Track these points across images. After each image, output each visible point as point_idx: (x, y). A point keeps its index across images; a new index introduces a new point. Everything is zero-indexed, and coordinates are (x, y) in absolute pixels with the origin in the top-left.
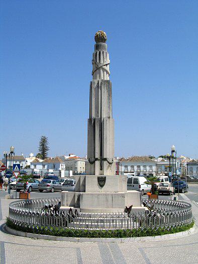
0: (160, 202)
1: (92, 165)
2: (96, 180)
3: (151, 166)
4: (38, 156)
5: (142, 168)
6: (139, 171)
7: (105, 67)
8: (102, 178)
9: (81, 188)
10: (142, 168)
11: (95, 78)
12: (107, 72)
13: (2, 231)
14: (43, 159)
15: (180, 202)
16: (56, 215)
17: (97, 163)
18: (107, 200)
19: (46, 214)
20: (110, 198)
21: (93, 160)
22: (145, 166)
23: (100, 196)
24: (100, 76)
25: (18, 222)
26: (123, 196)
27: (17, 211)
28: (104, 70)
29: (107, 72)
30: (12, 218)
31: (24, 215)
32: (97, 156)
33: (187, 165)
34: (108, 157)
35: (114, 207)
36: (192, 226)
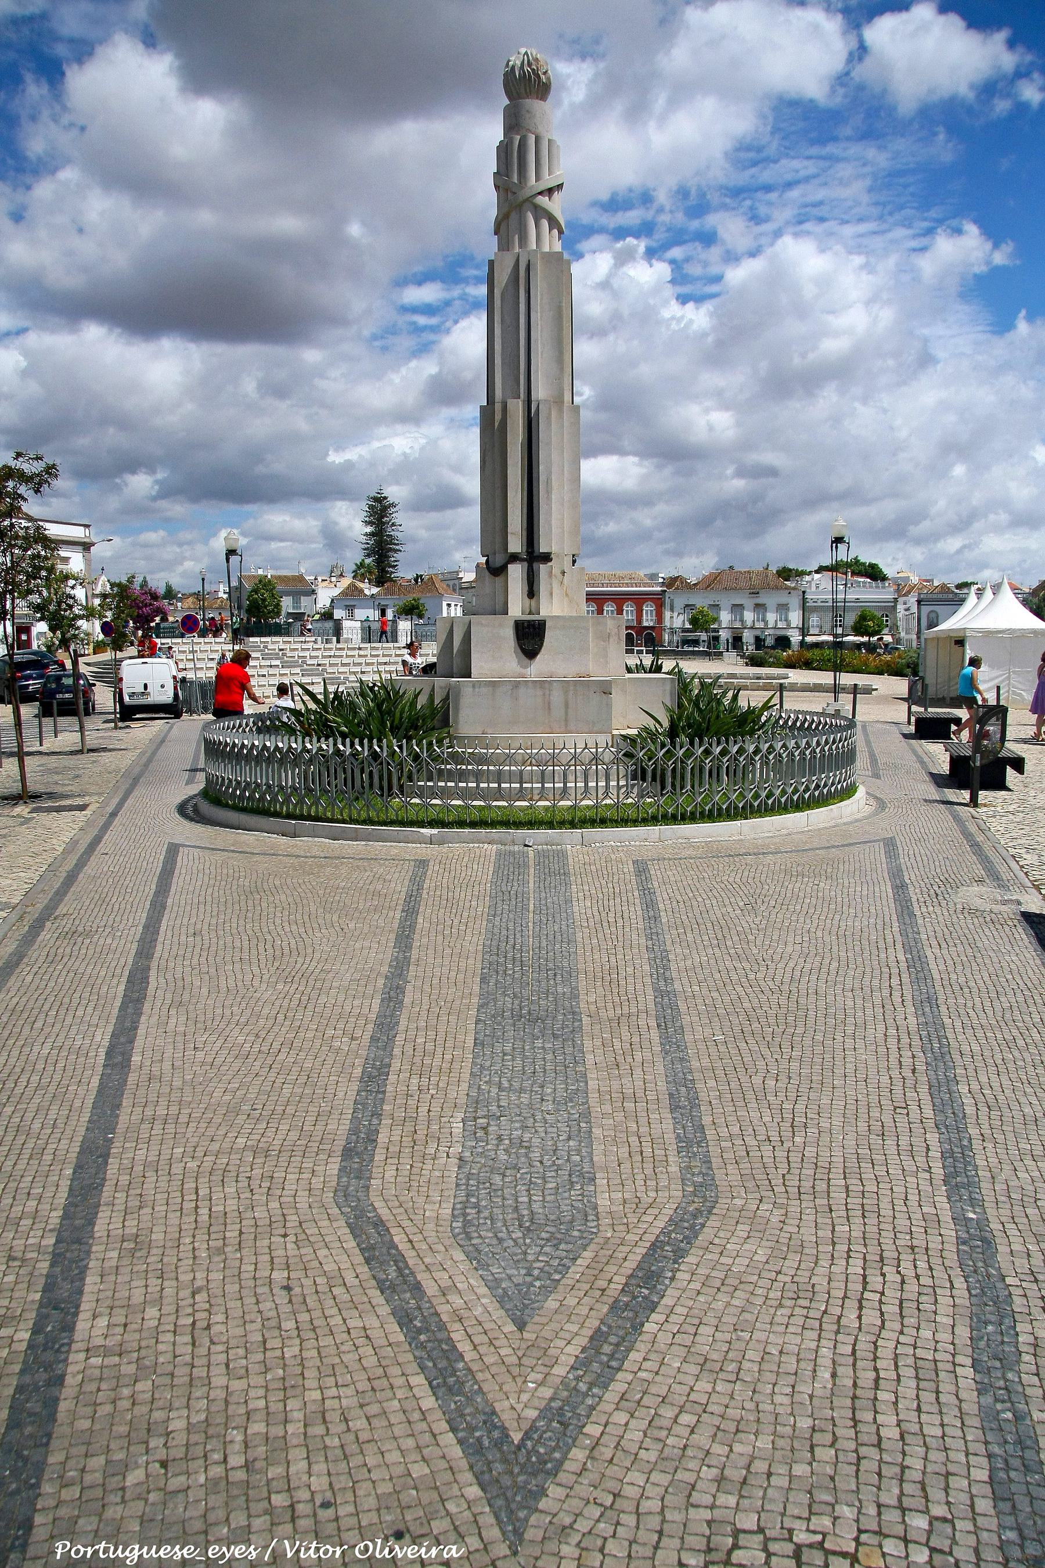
0: (786, 722)
1: (499, 580)
2: (509, 633)
3: (783, 608)
4: (360, 572)
5: (749, 616)
6: (738, 625)
7: (543, 201)
8: (531, 624)
9: (457, 663)
10: (749, 616)
11: (504, 246)
12: (561, 232)
13: (192, 820)
14: (380, 582)
15: (812, 713)
16: (375, 756)
17: (516, 572)
18: (548, 707)
19: (338, 752)
20: (557, 697)
21: (499, 560)
22: (760, 607)
23: (522, 690)
24: (523, 240)
25: (248, 784)
26: (605, 689)
27: (227, 744)
28: (541, 213)
29: (553, 222)
30: (225, 772)
31: (258, 759)
32: (516, 545)
33: (919, 602)
34: (554, 549)
35: (572, 727)
36: (848, 792)
